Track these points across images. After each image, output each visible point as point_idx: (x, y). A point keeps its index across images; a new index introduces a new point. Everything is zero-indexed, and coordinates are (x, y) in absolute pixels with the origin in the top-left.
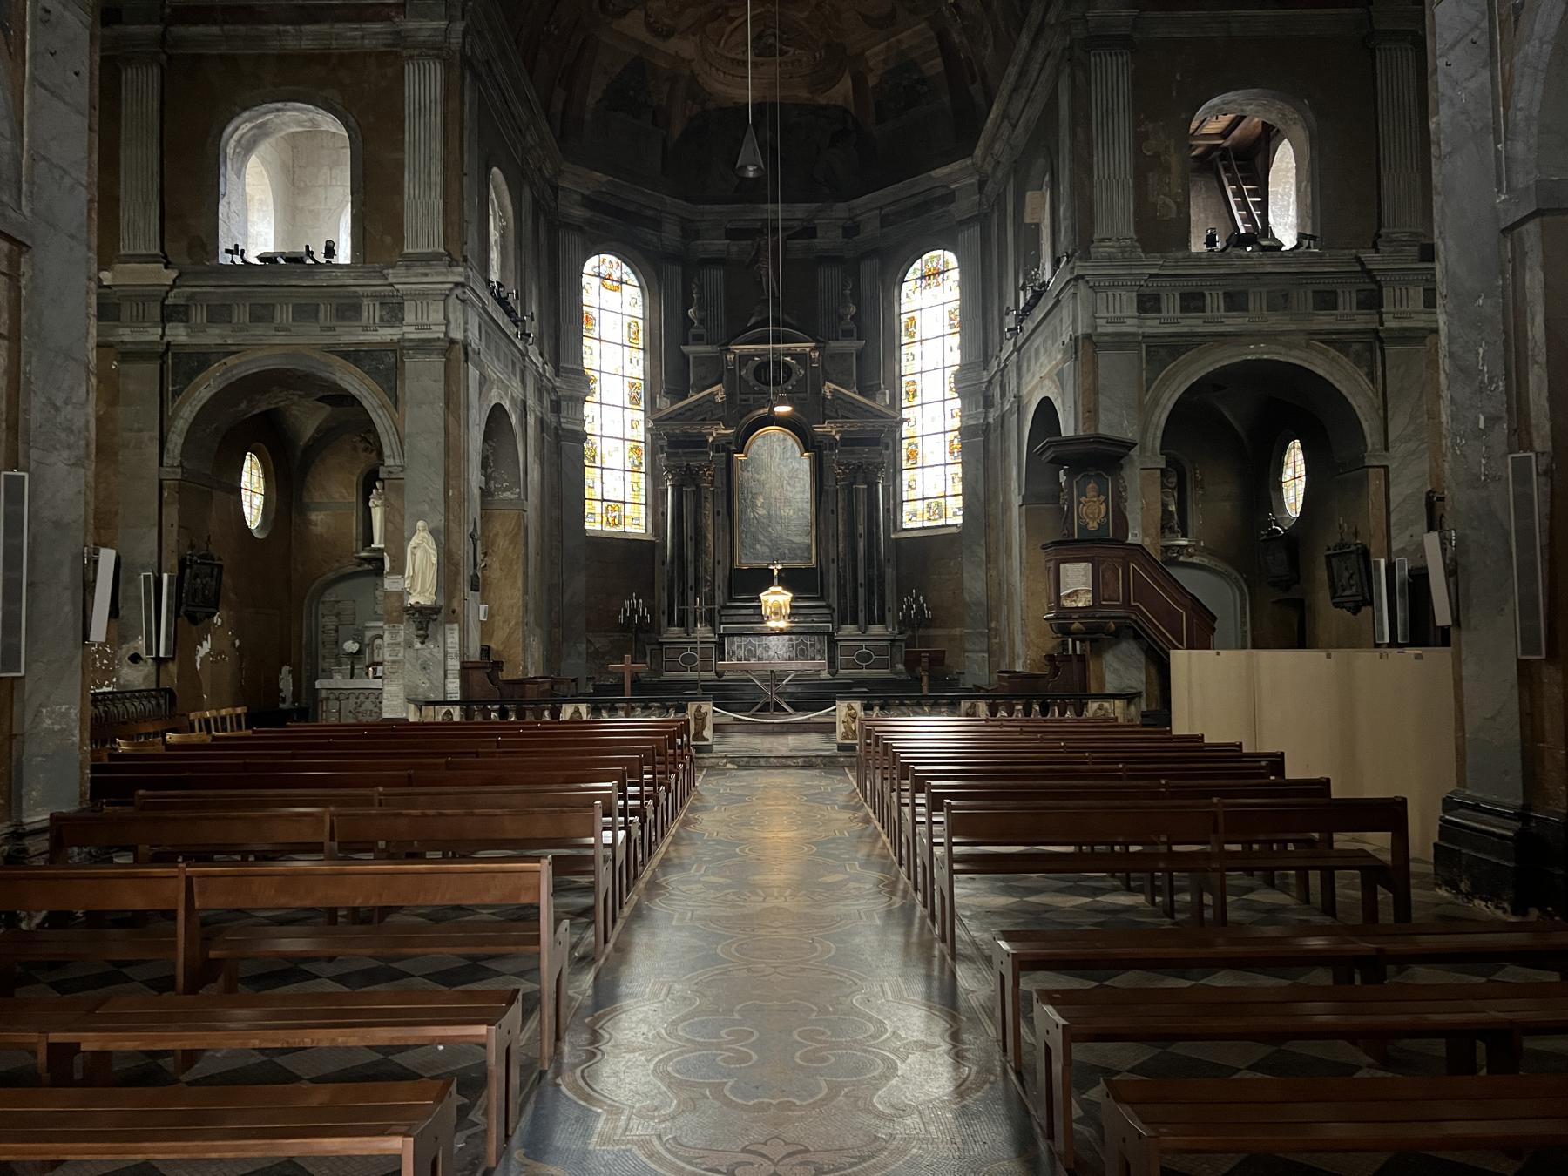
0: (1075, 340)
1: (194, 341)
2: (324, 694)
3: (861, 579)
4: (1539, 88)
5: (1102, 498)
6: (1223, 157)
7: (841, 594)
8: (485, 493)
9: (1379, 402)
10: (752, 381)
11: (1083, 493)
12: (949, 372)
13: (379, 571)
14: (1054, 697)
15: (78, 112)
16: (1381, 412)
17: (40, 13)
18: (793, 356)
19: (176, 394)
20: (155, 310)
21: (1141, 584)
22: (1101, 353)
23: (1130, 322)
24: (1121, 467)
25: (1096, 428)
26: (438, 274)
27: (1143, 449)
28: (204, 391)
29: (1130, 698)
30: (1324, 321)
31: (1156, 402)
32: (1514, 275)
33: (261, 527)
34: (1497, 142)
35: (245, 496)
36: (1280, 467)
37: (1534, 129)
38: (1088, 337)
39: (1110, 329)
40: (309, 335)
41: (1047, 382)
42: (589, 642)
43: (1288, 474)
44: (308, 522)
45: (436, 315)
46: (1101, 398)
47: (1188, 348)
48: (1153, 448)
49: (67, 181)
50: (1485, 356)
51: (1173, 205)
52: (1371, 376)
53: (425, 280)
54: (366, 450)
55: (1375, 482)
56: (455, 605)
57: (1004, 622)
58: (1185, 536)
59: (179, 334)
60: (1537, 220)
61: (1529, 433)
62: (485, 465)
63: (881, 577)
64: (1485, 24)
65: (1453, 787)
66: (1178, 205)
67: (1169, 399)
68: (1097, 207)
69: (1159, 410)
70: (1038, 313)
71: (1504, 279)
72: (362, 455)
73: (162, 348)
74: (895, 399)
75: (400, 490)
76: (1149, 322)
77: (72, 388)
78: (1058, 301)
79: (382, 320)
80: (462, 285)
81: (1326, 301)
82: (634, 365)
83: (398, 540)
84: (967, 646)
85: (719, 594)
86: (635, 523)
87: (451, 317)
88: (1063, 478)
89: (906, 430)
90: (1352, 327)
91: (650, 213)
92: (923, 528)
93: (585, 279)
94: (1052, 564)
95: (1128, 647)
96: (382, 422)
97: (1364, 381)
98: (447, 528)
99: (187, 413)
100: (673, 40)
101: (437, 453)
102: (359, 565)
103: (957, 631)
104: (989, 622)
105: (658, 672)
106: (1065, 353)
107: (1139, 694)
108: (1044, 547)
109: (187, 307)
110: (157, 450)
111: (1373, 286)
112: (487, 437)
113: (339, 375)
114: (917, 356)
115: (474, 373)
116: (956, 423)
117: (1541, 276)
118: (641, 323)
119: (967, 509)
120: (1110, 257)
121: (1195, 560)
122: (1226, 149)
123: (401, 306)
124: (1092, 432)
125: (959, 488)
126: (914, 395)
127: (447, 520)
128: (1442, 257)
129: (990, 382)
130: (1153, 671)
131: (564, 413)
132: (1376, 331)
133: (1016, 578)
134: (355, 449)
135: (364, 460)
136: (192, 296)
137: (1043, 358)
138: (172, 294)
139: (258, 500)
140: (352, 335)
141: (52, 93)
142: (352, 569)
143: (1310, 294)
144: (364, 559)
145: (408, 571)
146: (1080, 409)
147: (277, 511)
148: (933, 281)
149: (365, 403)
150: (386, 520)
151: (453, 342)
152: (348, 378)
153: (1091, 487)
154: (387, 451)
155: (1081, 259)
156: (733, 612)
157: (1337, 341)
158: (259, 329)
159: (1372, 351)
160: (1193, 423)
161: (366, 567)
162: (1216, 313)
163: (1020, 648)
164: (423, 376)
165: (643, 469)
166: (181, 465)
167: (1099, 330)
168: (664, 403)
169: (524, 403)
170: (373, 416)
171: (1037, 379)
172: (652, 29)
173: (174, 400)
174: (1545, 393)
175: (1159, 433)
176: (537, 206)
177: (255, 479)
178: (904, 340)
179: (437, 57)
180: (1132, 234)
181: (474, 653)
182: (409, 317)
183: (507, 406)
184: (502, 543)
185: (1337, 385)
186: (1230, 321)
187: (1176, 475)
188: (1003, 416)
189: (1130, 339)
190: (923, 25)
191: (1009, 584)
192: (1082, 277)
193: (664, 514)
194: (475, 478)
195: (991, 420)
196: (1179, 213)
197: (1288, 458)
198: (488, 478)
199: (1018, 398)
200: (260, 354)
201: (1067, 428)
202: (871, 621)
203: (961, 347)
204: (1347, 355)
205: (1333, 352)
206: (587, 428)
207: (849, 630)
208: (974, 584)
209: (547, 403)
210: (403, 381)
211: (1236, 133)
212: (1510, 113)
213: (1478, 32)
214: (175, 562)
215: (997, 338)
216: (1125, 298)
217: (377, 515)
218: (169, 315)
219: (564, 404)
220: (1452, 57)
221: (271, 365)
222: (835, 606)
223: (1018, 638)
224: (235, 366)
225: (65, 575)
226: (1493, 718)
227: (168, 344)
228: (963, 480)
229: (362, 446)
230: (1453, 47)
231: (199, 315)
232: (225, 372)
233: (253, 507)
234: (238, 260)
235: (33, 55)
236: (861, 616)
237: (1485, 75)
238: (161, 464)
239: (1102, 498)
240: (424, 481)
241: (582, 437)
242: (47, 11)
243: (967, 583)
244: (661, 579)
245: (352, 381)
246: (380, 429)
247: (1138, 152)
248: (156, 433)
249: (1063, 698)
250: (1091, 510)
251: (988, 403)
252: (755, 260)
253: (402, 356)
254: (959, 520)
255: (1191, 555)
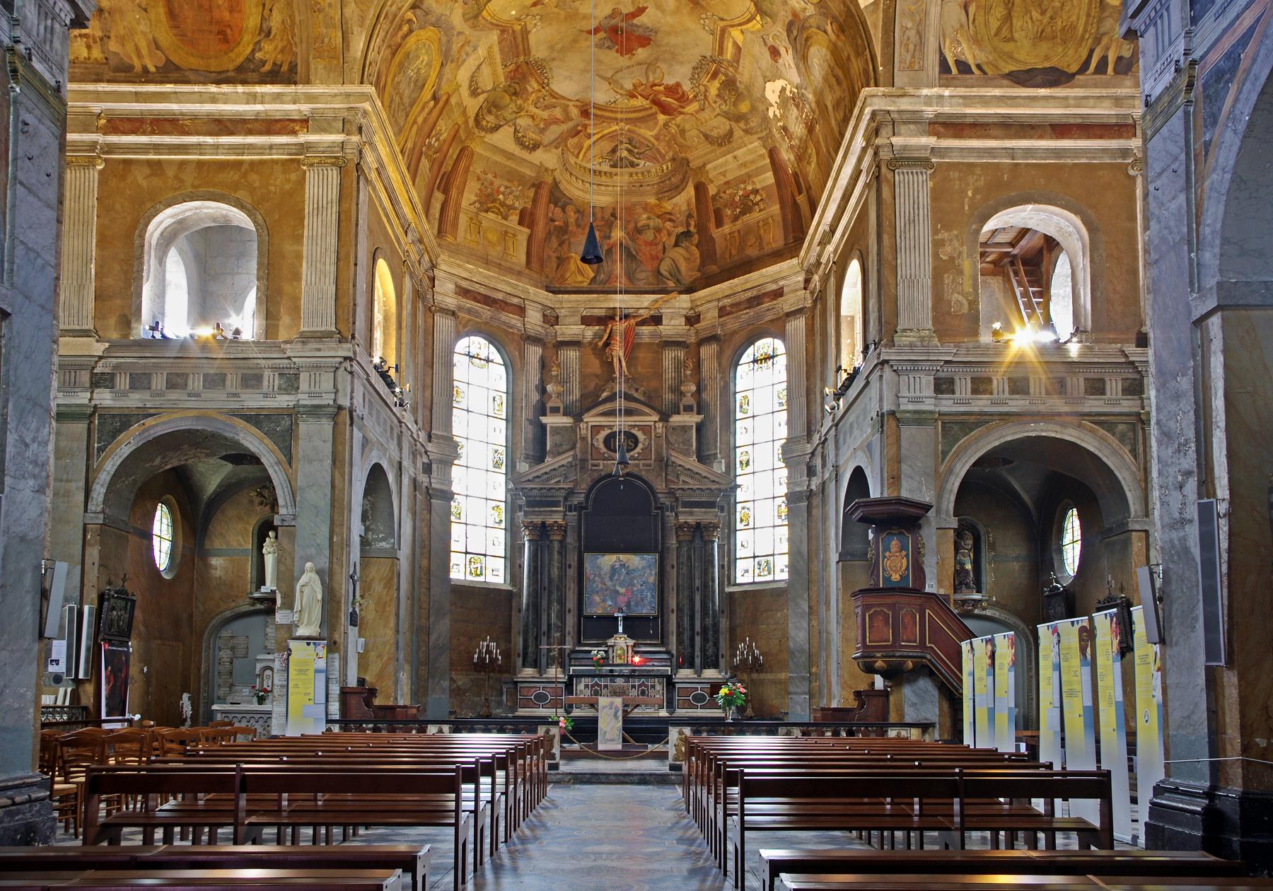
0: (881, 416)
1: (118, 404)
2: (219, 717)
3: (698, 628)
4: (1221, 208)
5: (904, 553)
6: (1012, 263)
7: (680, 642)
8: (364, 542)
9: (1140, 475)
10: (603, 449)
11: (887, 549)
12: (778, 444)
13: (270, 611)
14: (859, 725)
15: (49, 206)
16: (1143, 484)
17: (20, 125)
18: (641, 428)
19: (100, 450)
20: (85, 377)
21: (934, 627)
22: (903, 428)
23: (928, 401)
24: (920, 527)
25: (899, 491)
26: (330, 349)
27: (938, 512)
28: (125, 447)
29: (925, 727)
30: (1094, 405)
31: (950, 471)
32: (1203, 356)
33: (171, 567)
34: (1190, 251)
35: (156, 541)
36: (1061, 531)
37: (1218, 242)
38: (892, 413)
39: (911, 407)
40: (217, 400)
41: (860, 453)
42: (451, 679)
43: (1067, 539)
44: (207, 566)
45: (326, 382)
46: (904, 467)
47: (977, 425)
48: (947, 511)
49: (39, 261)
50: (1186, 425)
51: (966, 303)
52: (1134, 452)
53: (318, 354)
54: (261, 503)
55: (1137, 544)
56: (336, 637)
57: (823, 667)
58: (979, 591)
59: (104, 398)
60: (1219, 314)
61: (1213, 485)
62: (364, 518)
63: (716, 626)
64: (1183, 156)
65: (1162, 777)
66: (970, 303)
67: (962, 469)
68: (901, 303)
69: (952, 478)
70: (852, 392)
71: (1195, 360)
72: (259, 508)
73: (89, 411)
74: (731, 467)
75: (292, 537)
76: (944, 402)
77: (38, 430)
78: (867, 383)
79: (280, 388)
80: (351, 359)
81: (1096, 387)
82: (498, 433)
83: (288, 579)
84: (791, 689)
85: (568, 639)
86: (495, 574)
87: (340, 387)
88: (871, 536)
89: (740, 495)
90: (1117, 410)
91: (515, 301)
92: (754, 583)
93: (456, 358)
94: (859, 610)
95: (924, 684)
96: (277, 477)
97: (1128, 457)
98: (331, 569)
99: (110, 466)
100: (539, 152)
101: (325, 504)
102: (253, 605)
103: (783, 676)
104: (810, 666)
105: (513, 709)
106: (873, 426)
107: (932, 725)
108: (854, 595)
109: (113, 375)
110: (82, 498)
111: (1137, 376)
112: (367, 492)
113: (242, 435)
114: (750, 430)
115: (357, 435)
116: (784, 490)
117: (1222, 359)
118: (504, 396)
119: (792, 567)
120: (911, 345)
121: (988, 613)
122: (1015, 256)
123: (297, 376)
124: (895, 494)
125: (785, 547)
126: (747, 464)
127: (331, 562)
128: (1152, 342)
129: (813, 454)
130: (946, 706)
131: (434, 474)
132: (1139, 414)
133: (833, 627)
134: (251, 502)
135: (261, 513)
136: (116, 367)
137: (856, 432)
138: (100, 364)
139: (166, 546)
140: (253, 401)
141: (30, 191)
142: (248, 608)
143: (1081, 380)
144: (257, 599)
145: (297, 606)
146: (885, 475)
147: (183, 556)
148: (764, 365)
149: (263, 460)
150: (279, 562)
151: (340, 408)
152: (250, 438)
153: (895, 543)
154: (281, 502)
155: (886, 346)
156: (581, 655)
157: (1104, 422)
158: (174, 395)
159: (1134, 431)
160: (983, 491)
161: (259, 606)
162: (1001, 395)
163: (835, 689)
164: (314, 437)
165: (503, 525)
166: (103, 512)
167: (902, 407)
168: (523, 467)
169: (400, 463)
170: (270, 471)
171: (851, 450)
172: (520, 142)
173: (99, 456)
174: (1224, 452)
175: (953, 498)
176: (418, 295)
177: (165, 527)
178: (739, 415)
179: (333, 164)
180: (930, 326)
181: (352, 682)
182: (304, 386)
183: (385, 465)
184: (378, 588)
185: (1105, 459)
186: (1015, 403)
187: (968, 533)
188: (824, 483)
189: (930, 416)
190: (756, 144)
191: (828, 633)
192: (887, 362)
193: (521, 567)
194: (357, 528)
195: (813, 487)
196: (970, 309)
197: (1068, 524)
198: (367, 529)
199: (836, 467)
200: (174, 416)
201: (875, 493)
202: (706, 665)
203: (789, 423)
204: (1114, 435)
205: (1102, 431)
206: (454, 489)
207: (685, 673)
208: (798, 634)
209: (419, 465)
210: (297, 444)
211: (1023, 242)
212: (1201, 228)
213: (1177, 164)
214: (94, 596)
215: (819, 415)
216: (924, 381)
217: (269, 561)
218: (98, 381)
219: (434, 466)
220: (1158, 183)
221: (184, 426)
222: (674, 652)
223: (834, 679)
224: (156, 425)
225: (28, 580)
226: (1189, 717)
227: (95, 406)
228: (790, 540)
229: (258, 500)
230: (1160, 175)
231: (123, 382)
232: (143, 432)
233: (162, 553)
234: (158, 336)
235: (15, 159)
236: (698, 661)
237: (1182, 198)
238: (86, 511)
239: (904, 553)
240: (312, 529)
241: (448, 496)
242: (26, 124)
243: (792, 632)
244: (517, 625)
245: (252, 440)
246: (276, 482)
247: (936, 255)
248: (82, 484)
249: (866, 726)
250: (895, 565)
251: (811, 472)
252: (607, 344)
253: (297, 419)
254: (785, 576)
255: (984, 609)
